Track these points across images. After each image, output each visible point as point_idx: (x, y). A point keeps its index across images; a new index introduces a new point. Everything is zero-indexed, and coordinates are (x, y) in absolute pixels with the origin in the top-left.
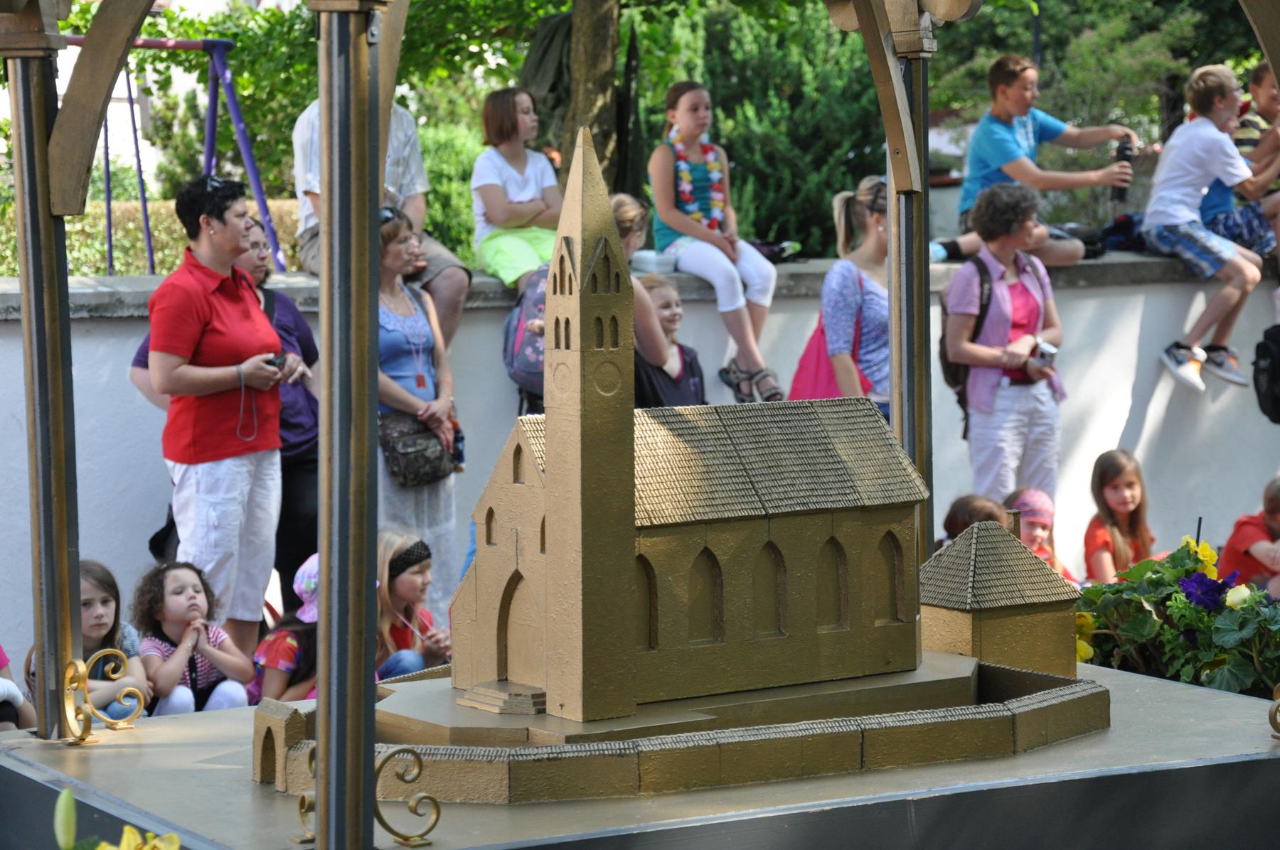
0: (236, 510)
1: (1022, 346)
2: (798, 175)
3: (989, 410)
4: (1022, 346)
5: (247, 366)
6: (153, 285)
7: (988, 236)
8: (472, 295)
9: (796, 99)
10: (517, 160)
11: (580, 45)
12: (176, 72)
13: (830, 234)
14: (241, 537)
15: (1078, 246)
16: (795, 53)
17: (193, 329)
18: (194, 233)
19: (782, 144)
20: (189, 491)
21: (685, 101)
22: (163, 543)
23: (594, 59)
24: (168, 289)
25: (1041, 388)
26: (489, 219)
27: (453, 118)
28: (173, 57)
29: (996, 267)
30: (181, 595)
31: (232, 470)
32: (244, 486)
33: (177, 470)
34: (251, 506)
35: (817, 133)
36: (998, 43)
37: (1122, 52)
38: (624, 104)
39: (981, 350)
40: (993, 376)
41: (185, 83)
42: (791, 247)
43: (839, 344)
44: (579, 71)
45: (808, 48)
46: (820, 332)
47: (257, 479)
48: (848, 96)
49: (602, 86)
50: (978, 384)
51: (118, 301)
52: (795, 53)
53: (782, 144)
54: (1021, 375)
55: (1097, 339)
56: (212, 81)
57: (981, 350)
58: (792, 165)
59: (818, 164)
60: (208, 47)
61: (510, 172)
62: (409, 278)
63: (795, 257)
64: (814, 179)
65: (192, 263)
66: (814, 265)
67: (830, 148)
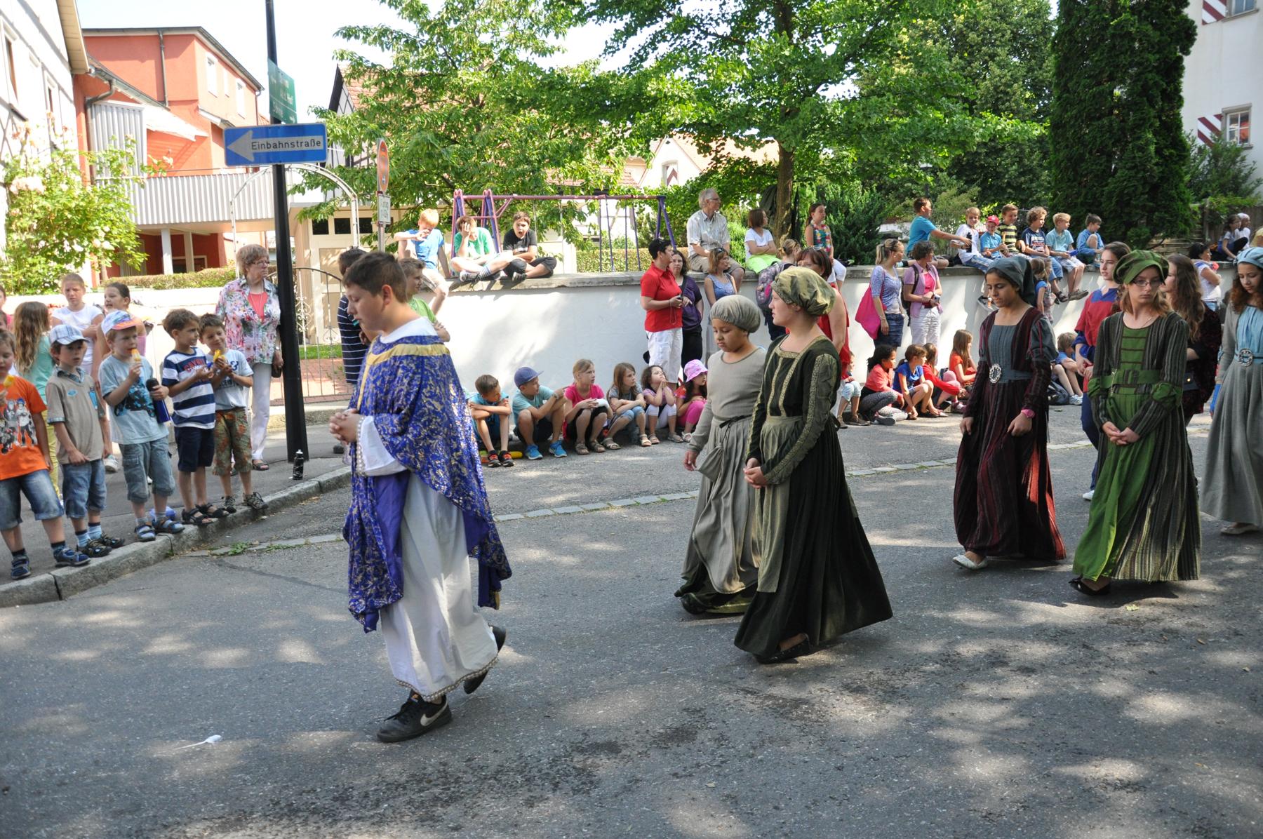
0: (669, 350)
1: (929, 295)
2: (847, 239)
3: (917, 317)
4: (929, 295)
5: (671, 300)
6: (642, 274)
7: (917, 259)
8: (746, 277)
9: (847, 213)
10: (760, 233)
11: (780, 194)
12: (647, 207)
13: (874, 257)
14: (1164, 630)
15: (946, 261)
16: (847, 198)
17: (655, 288)
18: (655, 257)
19: (842, 228)
20: (653, 341)
21: (818, 209)
22: (647, 357)
23: (784, 199)
24: (647, 276)
25: (934, 309)
26: (751, 253)
27: (732, 220)
28: (646, 202)
29: (920, 268)
30: (657, 375)
31: (667, 333)
32: (671, 339)
33: (650, 334)
34: (673, 346)
35: (854, 224)
36: (913, 195)
37: (955, 199)
38: (794, 213)
39: (915, 296)
40: (919, 305)
41: (648, 209)
42: (851, 261)
43: (876, 294)
44: (779, 203)
45: (851, 196)
46: (870, 289)
47: (675, 336)
48: (865, 212)
49: (787, 207)
50: (914, 308)
51: (632, 280)
52: (847, 198)
53: (842, 228)
54: (929, 305)
55: (950, 296)
56: (659, 209)
57: (915, 296)
58: (845, 235)
59: (854, 235)
60: (658, 198)
61: (757, 236)
62: (725, 271)
63: (855, 264)
64: (853, 239)
65: (654, 267)
66: (859, 267)
67: (858, 230)
